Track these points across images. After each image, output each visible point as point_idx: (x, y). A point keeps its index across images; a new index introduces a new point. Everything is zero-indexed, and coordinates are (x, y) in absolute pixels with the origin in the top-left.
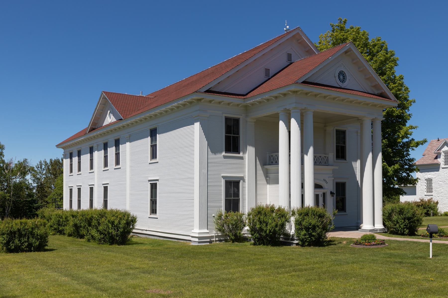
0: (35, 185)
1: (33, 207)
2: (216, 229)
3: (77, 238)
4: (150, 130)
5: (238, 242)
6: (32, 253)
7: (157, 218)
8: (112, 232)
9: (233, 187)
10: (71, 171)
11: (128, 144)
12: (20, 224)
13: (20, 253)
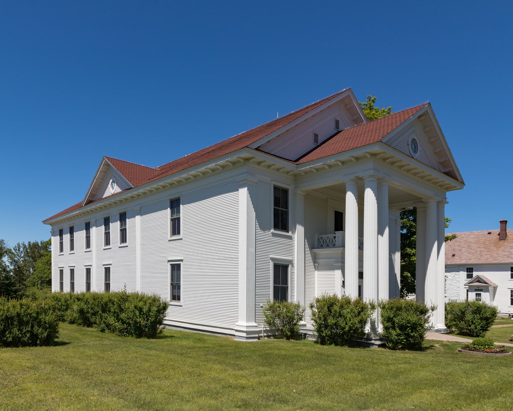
0: (12, 267)
1: (11, 291)
2: (266, 322)
3: (84, 326)
4: (170, 200)
5: (294, 339)
6: (39, 348)
7: (181, 306)
8: (140, 322)
9: (281, 271)
10: (62, 250)
11: (138, 218)
12: (19, 307)
13: (20, 348)
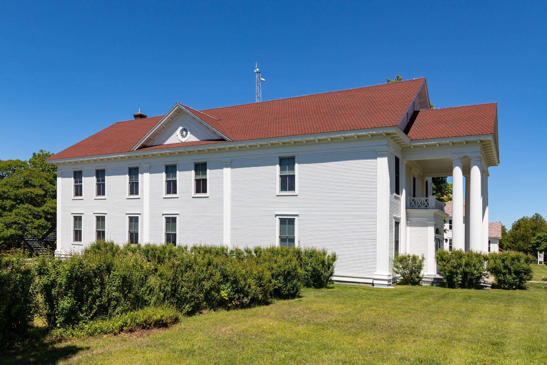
11: (227, 172)
